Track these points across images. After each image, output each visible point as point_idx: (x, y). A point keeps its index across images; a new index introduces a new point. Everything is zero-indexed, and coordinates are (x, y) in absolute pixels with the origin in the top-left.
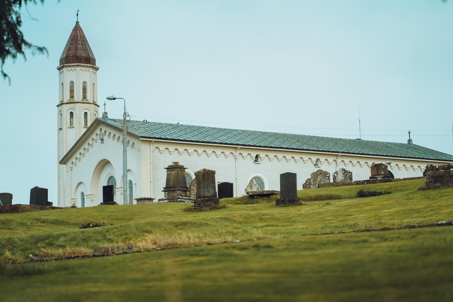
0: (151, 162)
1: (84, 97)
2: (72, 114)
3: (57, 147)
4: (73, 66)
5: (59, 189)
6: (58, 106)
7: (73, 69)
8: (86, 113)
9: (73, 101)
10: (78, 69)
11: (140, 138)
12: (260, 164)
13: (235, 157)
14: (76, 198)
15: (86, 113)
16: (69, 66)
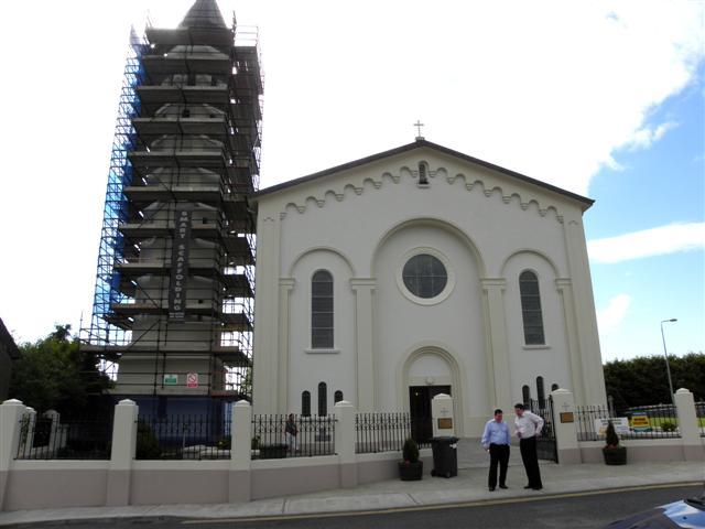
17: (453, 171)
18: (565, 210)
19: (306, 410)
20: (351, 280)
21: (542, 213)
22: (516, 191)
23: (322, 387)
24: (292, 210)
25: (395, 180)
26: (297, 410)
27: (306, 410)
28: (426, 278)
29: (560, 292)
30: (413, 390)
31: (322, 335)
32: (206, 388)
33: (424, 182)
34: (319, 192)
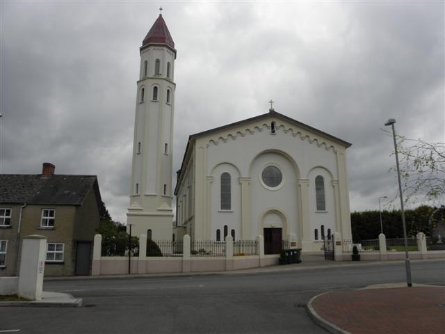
7: (160, 48)
17: (287, 126)
18: (338, 148)
19: (218, 238)
20: (239, 178)
21: (319, 146)
22: (307, 134)
23: (226, 227)
24: (212, 143)
25: (260, 130)
26: (214, 238)
27: (218, 238)
28: (272, 178)
29: (334, 186)
30: (265, 229)
31: (226, 203)
32: (129, 233)
33: (273, 132)
34: (225, 135)
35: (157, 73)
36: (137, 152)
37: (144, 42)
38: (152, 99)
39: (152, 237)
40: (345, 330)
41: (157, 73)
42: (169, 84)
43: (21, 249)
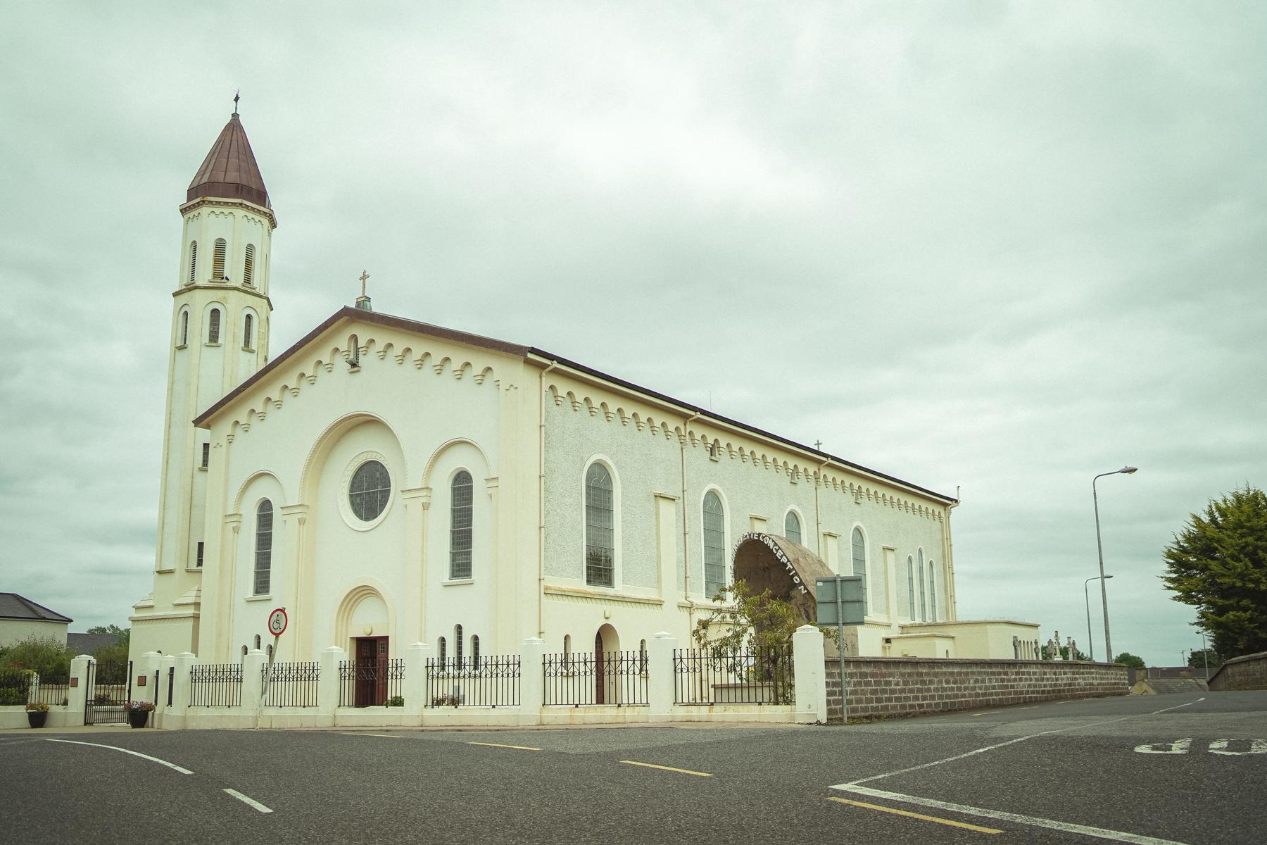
0: (543, 423)
1: (247, 280)
2: (215, 313)
3: (166, 392)
4: (226, 203)
5: (165, 491)
6: (175, 295)
7: (226, 211)
8: (249, 317)
9: (223, 284)
10: (240, 213)
11: (529, 352)
12: (717, 461)
13: (683, 438)
14: (241, 513)
15: (249, 317)
16: (218, 203)
35: (218, 274)
36: (179, 343)
37: (193, 192)
38: (206, 339)
39: (163, 724)
40: (833, 785)
41: (218, 274)
42: (250, 300)
43: (925, 500)
